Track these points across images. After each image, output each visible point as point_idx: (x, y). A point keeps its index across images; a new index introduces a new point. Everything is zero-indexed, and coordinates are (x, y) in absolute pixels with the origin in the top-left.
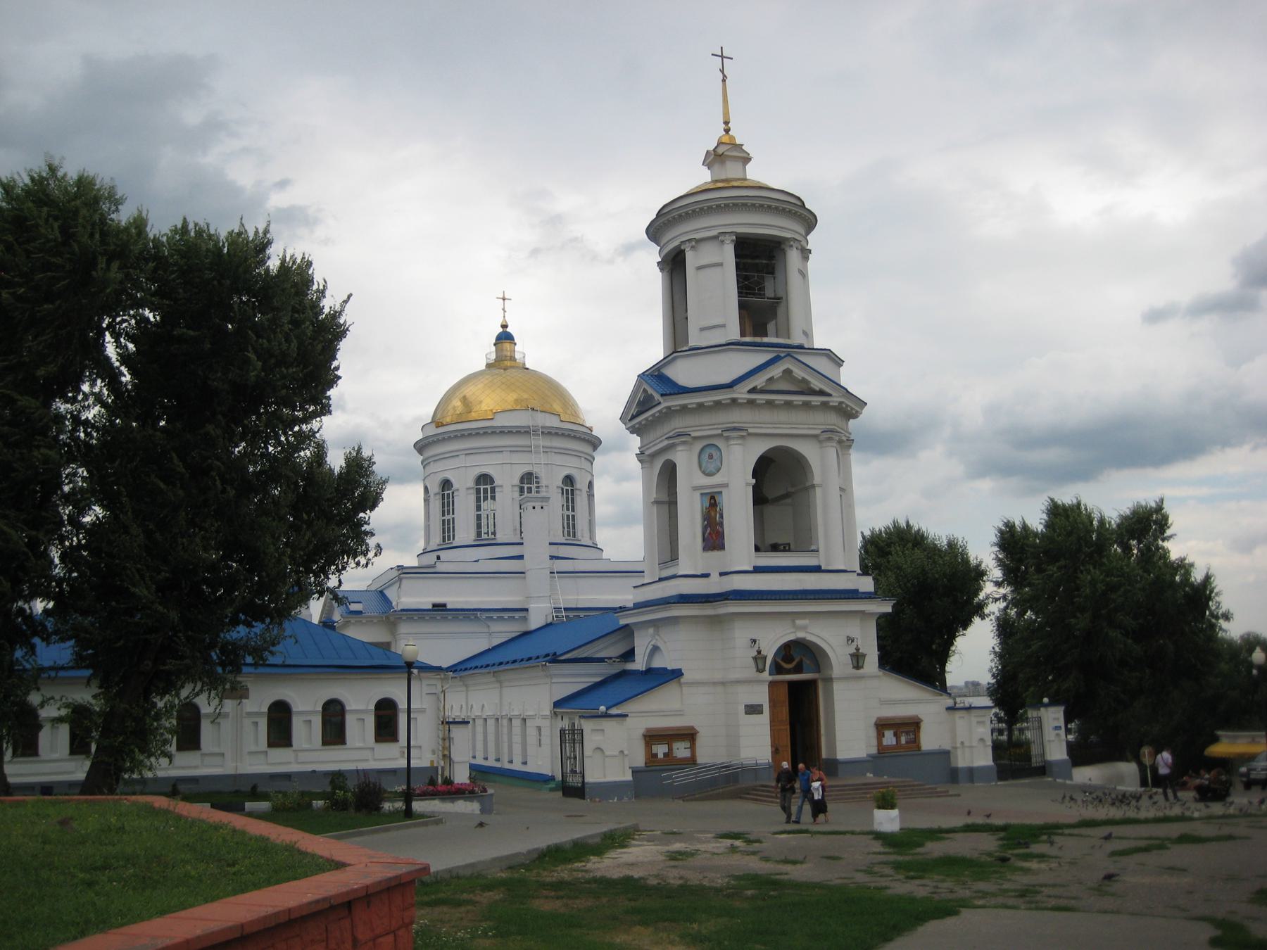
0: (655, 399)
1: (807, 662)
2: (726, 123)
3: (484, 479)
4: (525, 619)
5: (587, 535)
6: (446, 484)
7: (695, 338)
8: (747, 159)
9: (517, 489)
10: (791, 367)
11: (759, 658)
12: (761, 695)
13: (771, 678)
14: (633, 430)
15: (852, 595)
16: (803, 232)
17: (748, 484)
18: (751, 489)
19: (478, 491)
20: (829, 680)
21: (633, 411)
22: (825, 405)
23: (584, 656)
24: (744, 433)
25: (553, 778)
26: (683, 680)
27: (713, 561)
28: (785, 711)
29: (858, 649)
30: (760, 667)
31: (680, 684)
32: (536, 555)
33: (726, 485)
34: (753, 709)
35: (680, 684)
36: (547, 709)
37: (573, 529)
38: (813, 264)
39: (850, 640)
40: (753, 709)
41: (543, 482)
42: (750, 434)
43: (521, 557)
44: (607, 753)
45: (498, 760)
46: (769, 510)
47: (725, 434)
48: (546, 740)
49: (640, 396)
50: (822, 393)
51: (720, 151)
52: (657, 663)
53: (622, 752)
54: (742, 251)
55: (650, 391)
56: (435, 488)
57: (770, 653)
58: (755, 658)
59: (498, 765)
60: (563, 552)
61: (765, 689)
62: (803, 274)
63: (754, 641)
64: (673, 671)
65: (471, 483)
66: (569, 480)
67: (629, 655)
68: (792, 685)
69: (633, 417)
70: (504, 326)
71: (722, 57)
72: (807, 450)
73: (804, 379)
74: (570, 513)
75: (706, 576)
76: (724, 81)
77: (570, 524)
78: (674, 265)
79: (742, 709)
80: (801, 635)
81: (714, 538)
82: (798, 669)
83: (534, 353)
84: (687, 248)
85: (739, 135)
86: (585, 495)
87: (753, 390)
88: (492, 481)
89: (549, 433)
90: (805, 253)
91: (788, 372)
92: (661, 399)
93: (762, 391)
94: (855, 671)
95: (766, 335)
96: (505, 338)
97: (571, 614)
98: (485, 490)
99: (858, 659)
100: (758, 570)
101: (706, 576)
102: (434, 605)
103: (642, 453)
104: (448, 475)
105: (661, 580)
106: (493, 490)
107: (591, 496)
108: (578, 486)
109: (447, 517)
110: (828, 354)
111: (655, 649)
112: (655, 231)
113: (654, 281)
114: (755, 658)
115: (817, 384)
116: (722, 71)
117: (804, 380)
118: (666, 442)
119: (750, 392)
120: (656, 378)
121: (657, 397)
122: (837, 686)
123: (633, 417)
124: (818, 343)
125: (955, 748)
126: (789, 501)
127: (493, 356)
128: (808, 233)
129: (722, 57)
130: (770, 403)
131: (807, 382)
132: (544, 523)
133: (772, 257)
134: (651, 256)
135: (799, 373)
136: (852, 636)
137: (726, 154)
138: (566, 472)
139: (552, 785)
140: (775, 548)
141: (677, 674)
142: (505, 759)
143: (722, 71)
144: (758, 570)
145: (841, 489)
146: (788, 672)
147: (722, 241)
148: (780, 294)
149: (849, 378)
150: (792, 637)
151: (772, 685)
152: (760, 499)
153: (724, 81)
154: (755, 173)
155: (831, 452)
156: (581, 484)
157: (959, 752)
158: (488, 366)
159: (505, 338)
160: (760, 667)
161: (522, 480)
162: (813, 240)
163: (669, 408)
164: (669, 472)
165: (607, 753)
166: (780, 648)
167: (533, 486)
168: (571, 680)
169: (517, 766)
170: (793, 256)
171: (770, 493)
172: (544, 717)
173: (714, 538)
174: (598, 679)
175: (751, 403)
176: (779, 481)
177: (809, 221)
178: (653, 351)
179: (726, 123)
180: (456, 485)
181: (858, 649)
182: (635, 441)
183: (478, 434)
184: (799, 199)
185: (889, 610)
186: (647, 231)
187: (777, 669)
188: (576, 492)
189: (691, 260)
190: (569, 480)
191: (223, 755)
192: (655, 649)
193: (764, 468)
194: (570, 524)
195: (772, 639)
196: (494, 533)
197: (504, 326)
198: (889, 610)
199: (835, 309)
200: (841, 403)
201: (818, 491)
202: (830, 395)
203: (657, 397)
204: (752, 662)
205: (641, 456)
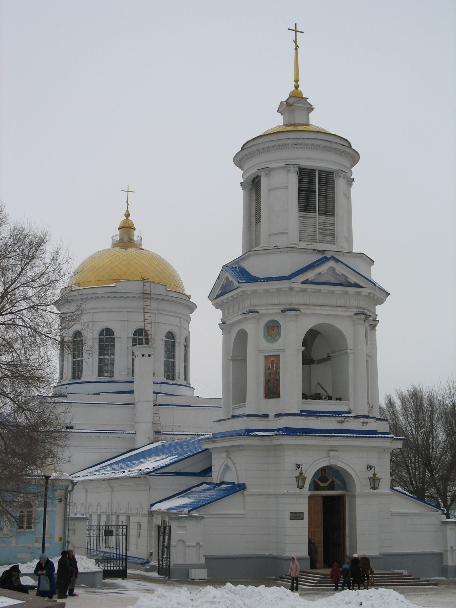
0: (235, 280)
1: (337, 482)
2: (297, 81)
4: (133, 439)
5: (182, 377)
8: (310, 109)
9: (131, 340)
11: (301, 478)
12: (302, 506)
13: (310, 493)
14: (217, 306)
16: (349, 166)
17: (298, 350)
20: (354, 497)
21: (218, 292)
23: (167, 471)
24: (298, 313)
26: (245, 492)
27: (271, 407)
28: (320, 517)
29: (375, 475)
30: (301, 484)
31: (244, 495)
32: (144, 388)
33: (283, 351)
34: (296, 516)
35: (244, 495)
37: (174, 368)
38: (355, 189)
39: (369, 467)
40: (296, 516)
43: (132, 392)
44: (188, 544)
46: (315, 368)
48: (144, 532)
49: (223, 281)
50: (356, 285)
51: (290, 101)
52: (228, 478)
53: (198, 544)
54: (302, 176)
55: (231, 279)
57: (309, 476)
58: (297, 478)
60: (165, 388)
61: (305, 501)
62: (348, 197)
63: (298, 466)
64: (239, 485)
66: (170, 335)
68: (325, 498)
69: (218, 296)
70: (127, 215)
71: (296, 31)
72: (345, 327)
73: (343, 275)
75: (266, 416)
76: (296, 49)
77: (170, 373)
78: (253, 185)
79: (288, 516)
80: (332, 462)
81: (272, 390)
82: (331, 487)
83: (150, 239)
84: (262, 174)
85: (306, 91)
86: (183, 348)
87: (306, 282)
88: (113, 334)
90: (350, 181)
92: (238, 285)
93: (312, 283)
94: (372, 491)
96: (127, 228)
99: (374, 482)
100: (304, 413)
103: (224, 323)
107: (187, 347)
108: (177, 340)
110: (362, 255)
111: (227, 468)
112: (239, 160)
113: (237, 197)
114: (297, 478)
115: (353, 279)
116: (295, 42)
118: (241, 317)
119: (303, 283)
122: (359, 502)
123: (218, 296)
124: (355, 250)
125: (447, 551)
127: (118, 238)
128: (352, 166)
129: (296, 31)
131: (346, 277)
132: (149, 367)
134: (237, 175)
135: (340, 269)
136: (371, 464)
137: (296, 104)
138: (168, 329)
140: (317, 397)
141: (241, 487)
143: (295, 42)
144: (304, 413)
145: (368, 355)
146: (323, 489)
149: (377, 275)
150: (327, 464)
152: (307, 360)
153: (296, 49)
154: (317, 120)
155: (362, 328)
156: (180, 341)
157: (449, 554)
158: (115, 245)
159: (127, 228)
160: (301, 484)
162: (357, 171)
163: (244, 292)
164: (241, 339)
165: (188, 544)
170: (340, 184)
171: (317, 354)
172: (143, 515)
173: (272, 390)
176: (319, 349)
177: (354, 157)
178: (234, 249)
179: (297, 81)
181: (375, 475)
182: (219, 314)
184: (346, 140)
186: (234, 160)
187: (315, 486)
188: (177, 344)
189: (264, 181)
190: (170, 335)
191: (186, 527)
192: (227, 468)
193: (311, 338)
194: (170, 373)
195: (312, 466)
197: (127, 215)
199: (372, 220)
200: (369, 293)
201: (351, 357)
202: (362, 287)
203: (236, 283)
204: (295, 480)
205: (223, 325)
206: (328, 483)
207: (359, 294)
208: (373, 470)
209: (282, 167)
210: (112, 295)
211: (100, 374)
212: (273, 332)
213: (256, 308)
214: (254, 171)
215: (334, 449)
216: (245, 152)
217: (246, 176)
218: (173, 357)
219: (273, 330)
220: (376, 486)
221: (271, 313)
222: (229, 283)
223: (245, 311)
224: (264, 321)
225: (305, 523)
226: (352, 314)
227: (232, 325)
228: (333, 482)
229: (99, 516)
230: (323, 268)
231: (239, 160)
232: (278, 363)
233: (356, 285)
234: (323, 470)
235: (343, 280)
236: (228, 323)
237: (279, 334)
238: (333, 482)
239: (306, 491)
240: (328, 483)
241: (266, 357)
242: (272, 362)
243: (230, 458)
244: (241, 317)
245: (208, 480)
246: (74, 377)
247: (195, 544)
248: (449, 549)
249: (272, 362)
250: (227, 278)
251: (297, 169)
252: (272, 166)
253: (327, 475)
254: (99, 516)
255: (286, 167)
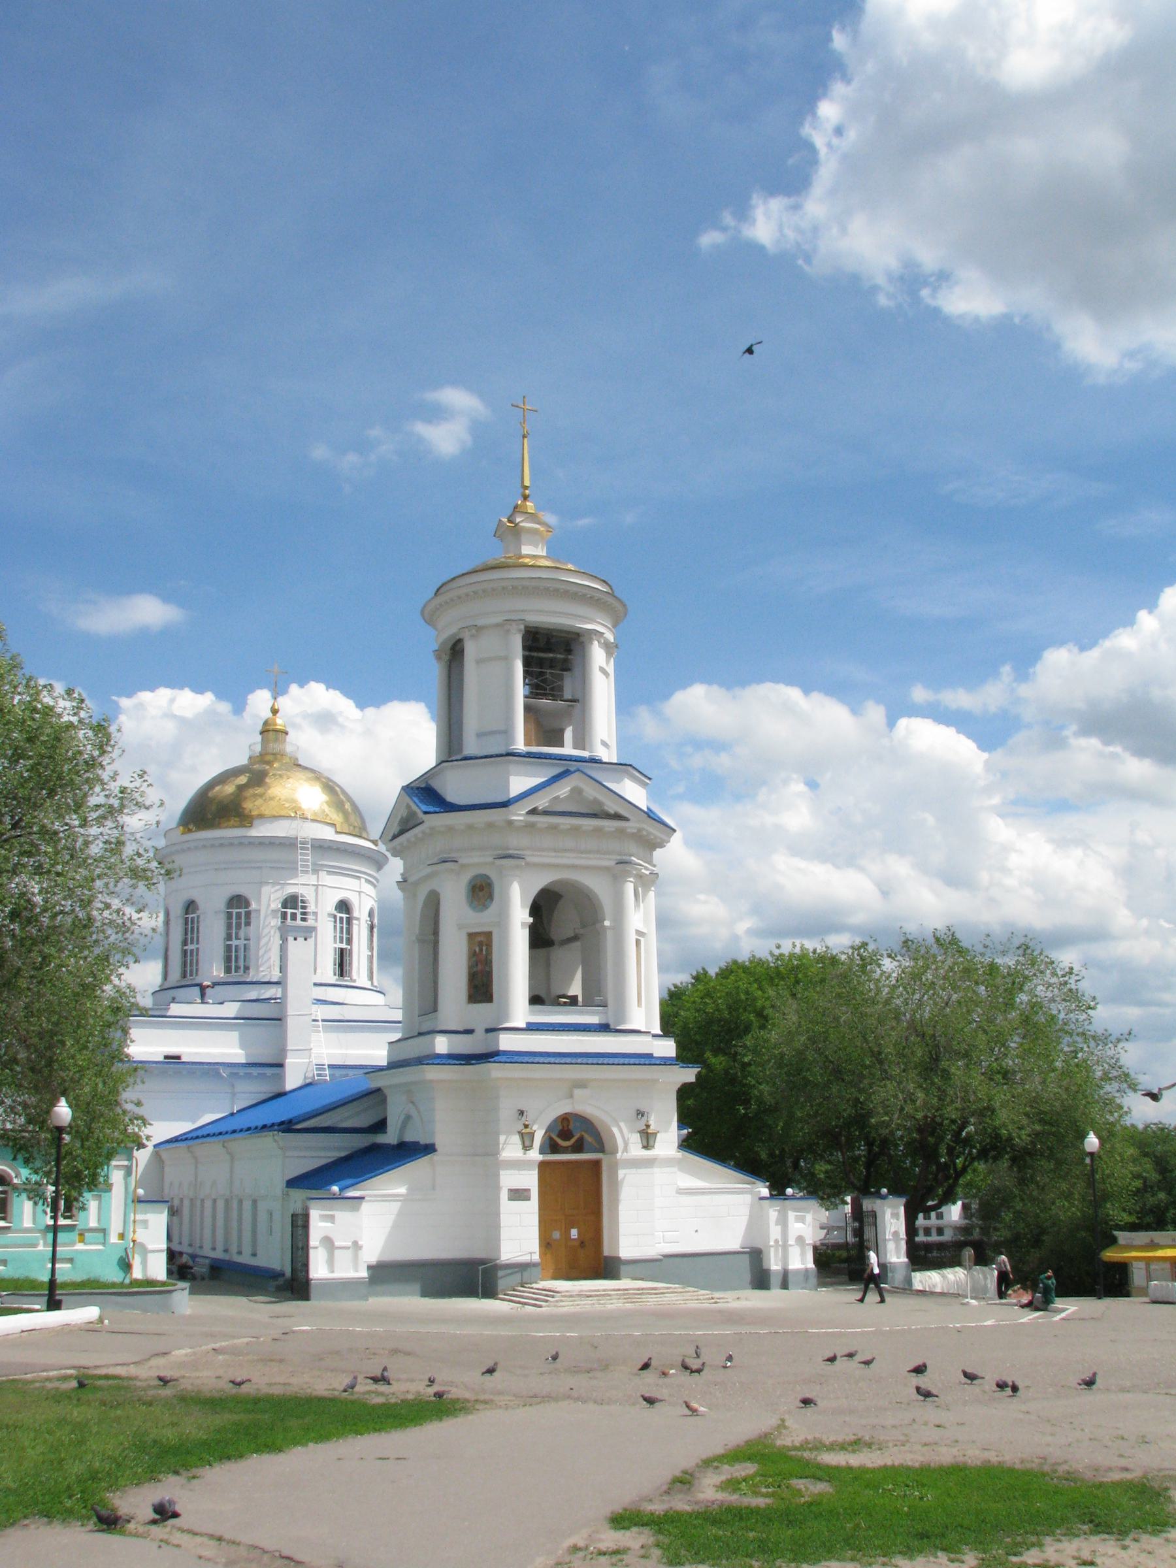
1: (588, 1138)
3: (292, 901)
6: (190, 906)
7: (471, 747)
10: (582, 785)
13: (541, 1158)
15: (646, 1059)
18: (527, 931)
19: (229, 916)
21: (395, 829)
22: (621, 832)
25: (280, 1275)
27: (480, 1014)
34: (519, 1195)
36: (280, 1185)
40: (519, 1195)
41: (311, 908)
42: (528, 864)
44: (337, 1244)
45: (226, 1251)
47: (499, 862)
49: (403, 812)
50: (617, 817)
52: (409, 1137)
55: (414, 807)
56: (177, 911)
59: (226, 1257)
63: (522, 1113)
65: (221, 904)
67: (380, 1126)
69: (395, 837)
72: (597, 885)
74: (234, 942)
75: (469, 1032)
79: (504, 1195)
81: (482, 986)
82: (578, 1147)
84: (466, 636)
87: (533, 812)
88: (247, 904)
89: (321, 847)
91: (576, 792)
93: (546, 813)
95: (562, 746)
97: (338, 1072)
98: (239, 915)
100: (532, 1028)
101: (469, 1032)
102: (166, 1057)
103: (405, 881)
104: (194, 894)
105: (420, 1034)
106: (248, 914)
108: (356, 914)
109: (189, 947)
115: (612, 807)
117: (596, 801)
118: (429, 870)
120: (426, 793)
121: (421, 815)
123: (395, 837)
126: (578, 944)
130: (554, 828)
131: (600, 803)
133: (569, 651)
135: (591, 792)
139: (281, 1281)
142: (247, 1250)
144: (532, 1028)
146: (565, 1150)
147: (508, 631)
148: (578, 696)
151: (543, 1165)
160: (527, 1143)
161: (285, 904)
163: (432, 828)
164: (433, 905)
166: (556, 1120)
167: (298, 912)
168: (312, 1152)
169: (245, 1259)
174: (343, 1154)
175: (530, 826)
180: (201, 904)
183: (231, 844)
185: (692, 1079)
187: (551, 1146)
189: (471, 650)
193: (544, 907)
196: (247, 968)
198: (692, 1079)
200: (640, 830)
202: (626, 819)
203: (421, 815)
206: (573, 1140)
207: (621, 832)
208: (644, 1119)
209: (497, 625)
210: (236, 841)
211: (228, 970)
212: (481, 894)
213: (453, 855)
214: (453, 630)
215: (581, 1084)
216: (441, 599)
217: (441, 640)
218: (349, 941)
219: (482, 891)
220: (651, 1143)
221: (477, 862)
222: (412, 815)
223: (435, 860)
224: (465, 878)
225: (533, 1204)
226: (612, 863)
227: (417, 884)
228: (581, 1139)
229: (215, 1201)
230: (563, 790)
231: (429, 617)
232: (489, 945)
233: (617, 817)
234: (565, 1119)
235: (596, 809)
236: (411, 880)
237: (490, 896)
238: (581, 1139)
239: (535, 1155)
240: (573, 1140)
241: (471, 936)
242: (480, 944)
243: (412, 1102)
244: (429, 870)
245: (381, 1139)
246: (184, 976)
247: (350, 1244)
248: (772, 1243)
249: (480, 944)
250: (408, 806)
251: (522, 627)
252: (481, 622)
253: (571, 1127)
254: (215, 1201)
255: (503, 627)
